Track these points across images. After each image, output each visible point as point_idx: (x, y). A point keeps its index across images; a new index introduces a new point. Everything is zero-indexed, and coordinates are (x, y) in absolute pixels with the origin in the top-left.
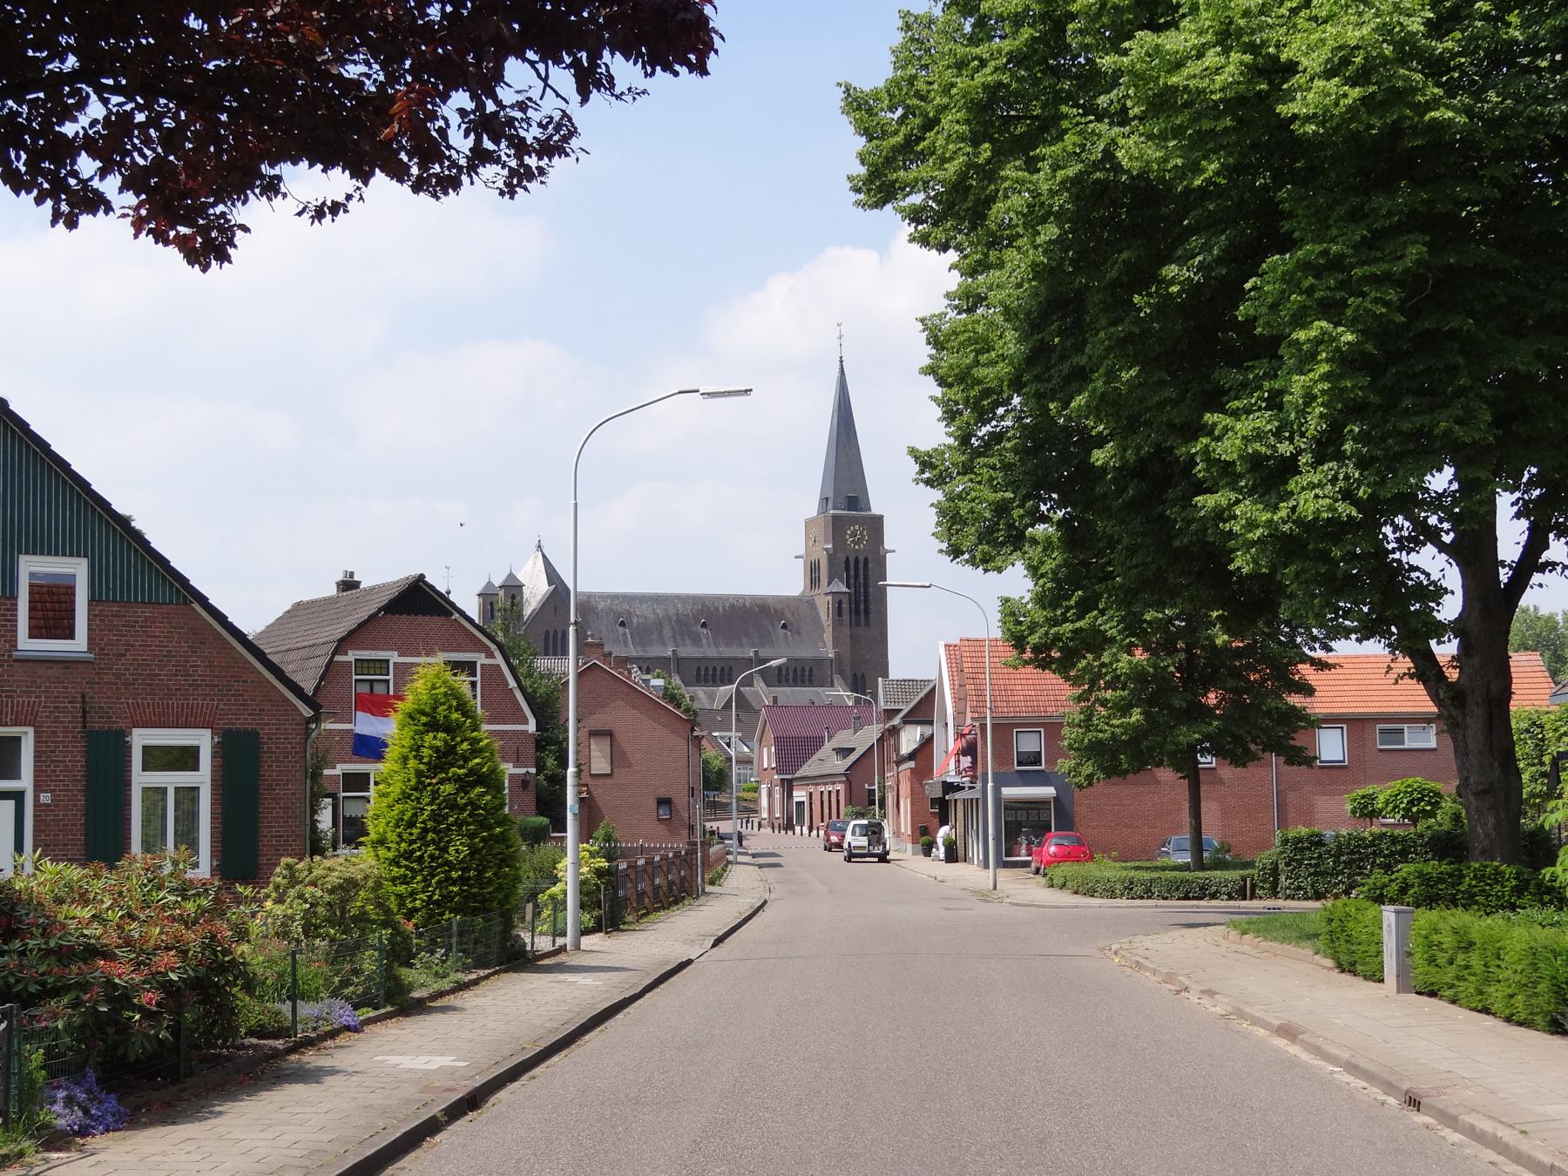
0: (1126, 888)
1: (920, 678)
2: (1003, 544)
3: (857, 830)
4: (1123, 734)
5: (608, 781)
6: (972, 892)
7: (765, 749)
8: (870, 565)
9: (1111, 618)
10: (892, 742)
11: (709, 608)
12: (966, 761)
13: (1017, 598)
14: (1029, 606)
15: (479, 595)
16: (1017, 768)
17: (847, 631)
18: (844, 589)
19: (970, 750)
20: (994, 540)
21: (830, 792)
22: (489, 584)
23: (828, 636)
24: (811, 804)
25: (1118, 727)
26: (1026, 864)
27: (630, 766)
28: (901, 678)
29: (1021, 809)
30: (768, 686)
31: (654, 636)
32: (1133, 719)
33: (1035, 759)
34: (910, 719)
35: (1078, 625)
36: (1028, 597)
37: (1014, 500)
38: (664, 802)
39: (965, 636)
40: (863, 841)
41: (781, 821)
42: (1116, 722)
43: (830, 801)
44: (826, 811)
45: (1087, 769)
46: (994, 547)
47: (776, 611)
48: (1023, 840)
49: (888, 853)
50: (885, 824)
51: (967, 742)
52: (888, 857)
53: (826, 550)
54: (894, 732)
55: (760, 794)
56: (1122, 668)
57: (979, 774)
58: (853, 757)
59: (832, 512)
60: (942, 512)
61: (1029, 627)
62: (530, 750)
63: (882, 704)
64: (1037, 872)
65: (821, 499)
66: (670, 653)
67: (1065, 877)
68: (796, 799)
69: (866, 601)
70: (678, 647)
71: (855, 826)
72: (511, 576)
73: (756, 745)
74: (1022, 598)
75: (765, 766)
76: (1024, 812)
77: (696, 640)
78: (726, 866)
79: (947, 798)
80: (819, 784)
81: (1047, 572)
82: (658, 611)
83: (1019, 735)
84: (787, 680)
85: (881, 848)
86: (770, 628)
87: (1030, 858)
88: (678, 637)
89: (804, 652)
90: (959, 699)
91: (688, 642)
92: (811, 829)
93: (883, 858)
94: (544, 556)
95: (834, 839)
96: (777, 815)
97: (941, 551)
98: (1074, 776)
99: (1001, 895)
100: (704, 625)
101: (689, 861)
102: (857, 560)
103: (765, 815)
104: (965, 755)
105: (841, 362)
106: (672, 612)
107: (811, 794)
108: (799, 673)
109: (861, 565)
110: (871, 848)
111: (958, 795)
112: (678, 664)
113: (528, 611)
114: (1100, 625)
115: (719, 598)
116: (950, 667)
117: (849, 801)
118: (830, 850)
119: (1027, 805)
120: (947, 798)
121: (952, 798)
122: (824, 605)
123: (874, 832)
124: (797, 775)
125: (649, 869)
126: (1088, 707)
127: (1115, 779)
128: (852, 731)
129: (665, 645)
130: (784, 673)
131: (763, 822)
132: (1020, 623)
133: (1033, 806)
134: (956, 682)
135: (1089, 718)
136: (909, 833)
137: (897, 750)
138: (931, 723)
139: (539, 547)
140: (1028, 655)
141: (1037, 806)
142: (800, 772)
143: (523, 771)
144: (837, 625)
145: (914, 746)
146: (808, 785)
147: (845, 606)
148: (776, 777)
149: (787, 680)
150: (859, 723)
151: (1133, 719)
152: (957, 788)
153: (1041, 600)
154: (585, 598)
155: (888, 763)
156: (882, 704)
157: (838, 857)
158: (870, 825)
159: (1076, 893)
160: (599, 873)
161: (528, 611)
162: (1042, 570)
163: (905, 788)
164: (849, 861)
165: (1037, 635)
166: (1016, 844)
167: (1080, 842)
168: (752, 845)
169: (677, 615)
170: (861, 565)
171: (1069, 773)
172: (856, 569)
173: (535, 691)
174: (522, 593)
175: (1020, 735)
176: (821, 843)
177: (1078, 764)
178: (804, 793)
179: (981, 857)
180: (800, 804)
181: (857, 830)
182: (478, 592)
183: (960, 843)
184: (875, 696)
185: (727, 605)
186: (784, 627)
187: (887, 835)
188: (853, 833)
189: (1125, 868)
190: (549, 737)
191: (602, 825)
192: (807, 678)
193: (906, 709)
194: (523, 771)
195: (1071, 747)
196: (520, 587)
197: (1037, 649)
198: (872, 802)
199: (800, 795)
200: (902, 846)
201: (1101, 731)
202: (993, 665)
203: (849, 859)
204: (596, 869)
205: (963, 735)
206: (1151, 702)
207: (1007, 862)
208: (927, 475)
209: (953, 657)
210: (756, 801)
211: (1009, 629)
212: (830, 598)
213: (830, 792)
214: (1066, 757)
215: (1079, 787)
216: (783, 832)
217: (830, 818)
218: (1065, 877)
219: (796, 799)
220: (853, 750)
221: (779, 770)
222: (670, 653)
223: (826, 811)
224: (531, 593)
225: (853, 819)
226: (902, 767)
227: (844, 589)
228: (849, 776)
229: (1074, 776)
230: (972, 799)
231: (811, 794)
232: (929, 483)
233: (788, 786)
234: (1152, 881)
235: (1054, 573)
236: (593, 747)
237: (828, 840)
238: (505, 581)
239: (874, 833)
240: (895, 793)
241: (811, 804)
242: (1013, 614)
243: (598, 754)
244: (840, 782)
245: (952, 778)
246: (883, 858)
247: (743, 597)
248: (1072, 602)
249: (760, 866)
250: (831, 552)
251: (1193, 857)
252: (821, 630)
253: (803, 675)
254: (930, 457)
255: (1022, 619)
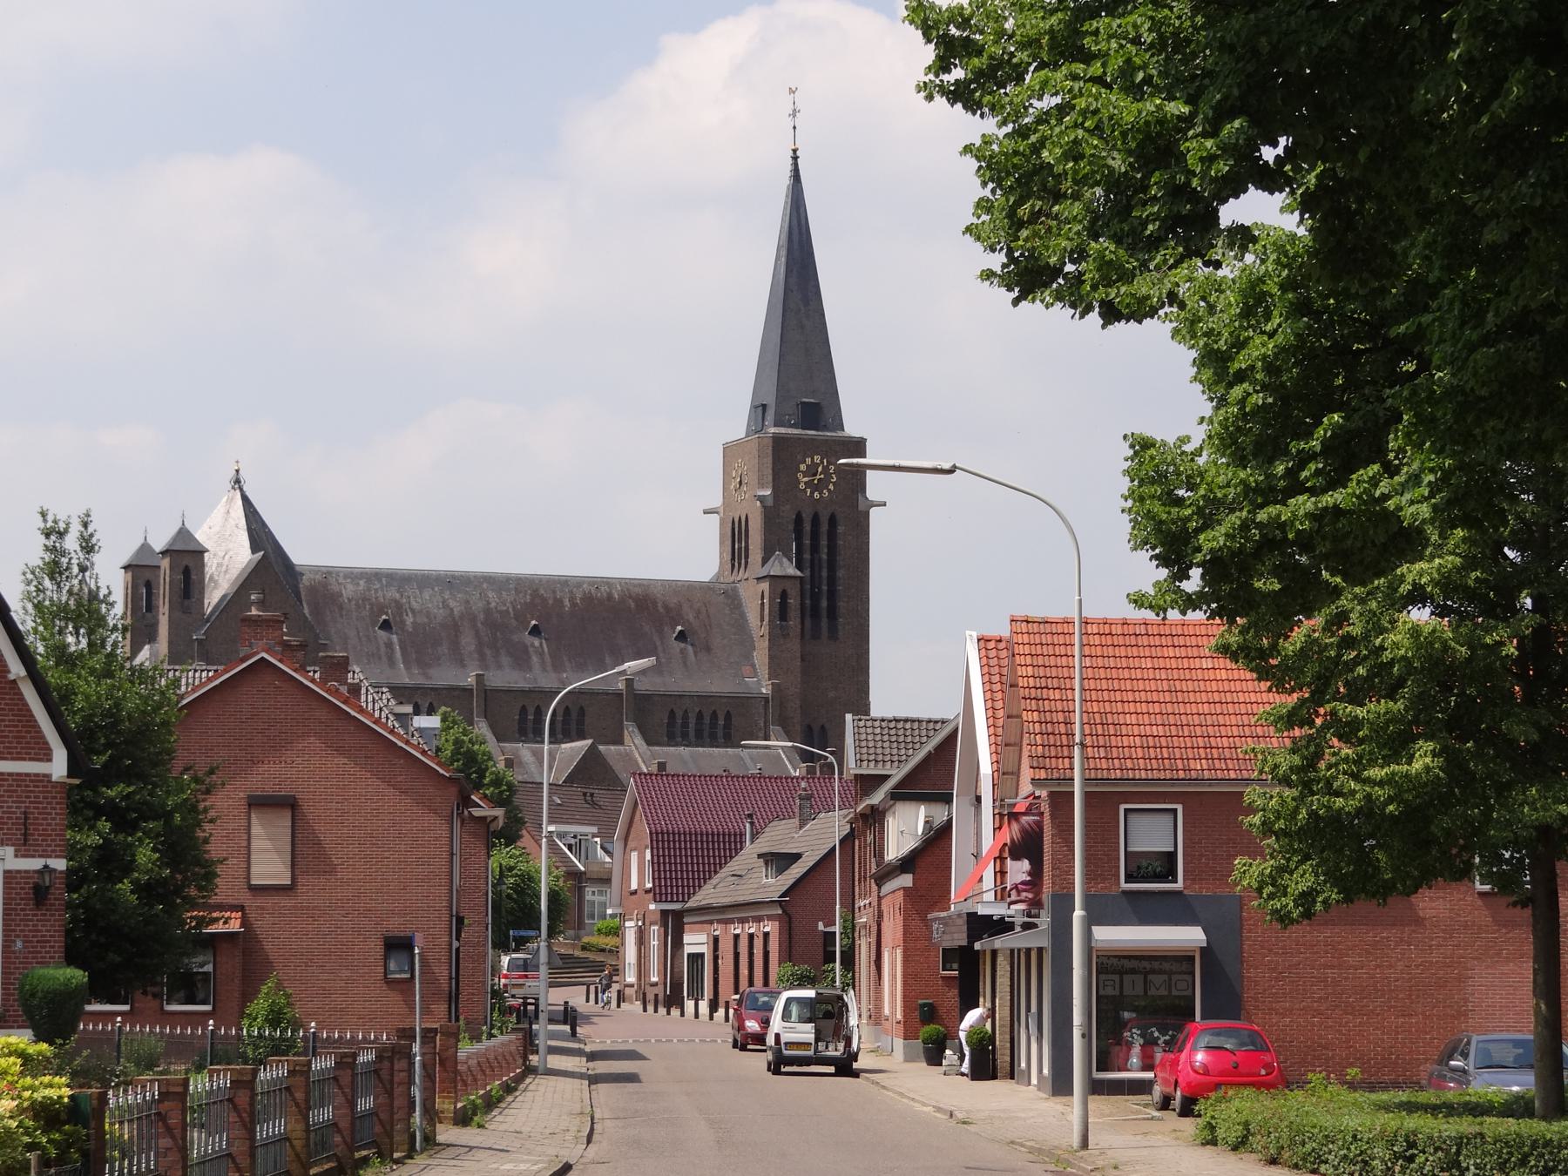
0: (1396, 1156)
1: (924, 715)
2: (1155, 243)
3: (794, 1009)
4: (1390, 800)
5: (285, 901)
6: (1031, 1151)
7: (634, 856)
8: (840, 529)
9: (1415, 479)
10: (870, 839)
11: (544, 600)
12: (1019, 870)
13: (1171, 440)
14: (1201, 461)
15: (126, 568)
16: (1124, 886)
17: (794, 646)
18: (791, 570)
19: (1027, 846)
20: (1133, 232)
21: (751, 936)
22: (145, 548)
23: (761, 657)
24: (716, 958)
25: (1381, 783)
26: (1140, 1088)
27: (331, 870)
28: (890, 715)
29: (1133, 971)
30: (649, 743)
31: (444, 649)
32: (1417, 765)
33: (1164, 866)
34: (908, 791)
35: (1328, 499)
36: (1198, 435)
37: (1188, 120)
38: (398, 945)
39: (1021, 613)
40: (806, 1033)
41: (659, 990)
42: (1376, 773)
43: (751, 954)
44: (744, 971)
45: (1302, 880)
46: (1132, 250)
47: (666, 607)
48: (1135, 1038)
49: (855, 1057)
50: (850, 998)
51: (1023, 831)
52: (855, 1066)
53: (761, 499)
54: (874, 819)
55: (623, 939)
56: (1396, 645)
57: (1046, 897)
58: (797, 871)
59: (772, 430)
60: (993, 166)
61: (1200, 512)
62: (57, 816)
63: (852, 764)
64: (1165, 1104)
65: (754, 407)
66: (471, 680)
67: (1246, 1124)
68: (688, 950)
69: (832, 594)
70: (486, 668)
71: (789, 1001)
72: (183, 533)
73: (617, 847)
74: (1184, 440)
75: (634, 886)
76: (1139, 979)
77: (521, 659)
78: (520, 1079)
79: (977, 946)
80: (731, 921)
81: (1252, 368)
82: (452, 604)
83: (1132, 817)
84: (685, 735)
85: (841, 1046)
86: (656, 638)
87: (1149, 1075)
88: (488, 652)
89: (715, 683)
90: (1005, 746)
91: (505, 660)
92: (714, 1006)
93: (845, 1067)
94: (246, 501)
95: (752, 1025)
96: (654, 979)
97: (988, 275)
98: (1271, 896)
99: (1100, 1163)
100: (535, 631)
101: (385, 1074)
102: (816, 520)
103: (631, 978)
104: (1016, 856)
105: (795, 158)
106: (478, 606)
107: (716, 940)
108: (707, 720)
109: (824, 528)
110: (821, 1046)
111: (1001, 942)
112: (489, 701)
113: (213, 598)
114: (1385, 497)
115: (564, 582)
116: (988, 683)
117: (788, 955)
118: (743, 1048)
119: (1146, 964)
120: (977, 946)
121: (988, 947)
122: (754, 598)
123: (827, 1015)
124: (691, 904)
125: (345, 1079)
126: (1310, 738)
127: (1363, 906)
128: (796, 821)
129: (464, 666)
130: (679, 721)
131: (628, 991)
132: (1179, 502)
133: (1156, 965)
134: (1000, 713)
135: (1311, 762)
136: (899, 1016)
137: (879, 852)
138: (947, 799)
139: (238, 481)
140: (1194, 583)
141: (1166, 966)
142: (694, 898)
143: (35, 864)
144: (777, 636)
145: (910, 845)
146: (711, 922)
147: (793, 601)
148: (652, 907)
149: (685, 735)
150: (810, 806)
151: (1417, 765)
152: (1001, 926)
153: (1230, 440)
154: (318, 577)
155: (863, 878)
156: (852, 764)
157: (757, 1062)
158: (820, 998)
159: (1273, 1161)
160: (46, 1114)
161: (213, 598)
162: (1240, 363)
163: (893, 929)
164: (777, 1072)
165: (1221, 530)
166: (1118, 1044)
167: (1258, 1043)
168: (597, 1035)
169: (488, 611)
170: (824, 528)
171: (1260, 890)
172: (815, 535)
173: (117, 705)
174: (201, 565)
175: (1133, 818)
176: (727, 1033)
177: (1281, 870)
178: (703, 938)
179: (1046, 1071)
180: (696, 958)
181: (794, 1009)
182: (124, 560)
183: (1001, 1041)
184: (840, 755)
185: (579, 596)
186: (682, 637)
187: (853, 1021)
188: (786, 1016)
189: (1387, 1108)
190: (145, 803)
191: (264, 989)
192: (720, 733)
193: (897, 774)
194: (35, 864)
195: (1267, 828)
196: (199, 553)
197: (1216, 568)
198: (830, 958)
199: (695, 941)
200: (885, 1041)
201: (1338, 794)
202: (1088, 662)
203: (775, 1068)
204: (34, 1103)
205: (1014, 816)
206: (1459, 725)
207: (1102, 1082)
208: (958, 74)
209: (993, 662)
210: (616, 952)
211: (1149, 515)
212: (765, 586)
213: (751, 936)
214: (1255, 852)
215: (1281, 919)
216: (662, 1010)
217: (751, 984)
218: (1246, 1124)
219: (688, 950)
220: (797, 857)
221: (658, 894)
222: (471, 680)
223: (744, 971)
224: (220, 565)
225: (786, 989)
226: (888, 887)
227: (791, 570)
228: (790, 907)
229: (1271, 896)
230: (1029, 950)
231: (716, 940)
232: (959, 95)
233: (675, 925)
234: (1461, 1141)
235: (1271, 368)
236: (256, 829)
237: (741, 1027)
238: (170, 545)
239: (828, 1015)
240: (873, 939)
241: (716, 958)
242: (1160, 478)
243: (268, 845)
244: (770, 918)
245: (988, 906)
246: (845, 1067)
247: (607, 581)
248: (1315, 444)
249: (594, 1080)
250: (770, 503)
251: (1540, 1081)
252: (748, 645)
253: (714, 724)
254: (965, 23)
255: (1181, 492)
